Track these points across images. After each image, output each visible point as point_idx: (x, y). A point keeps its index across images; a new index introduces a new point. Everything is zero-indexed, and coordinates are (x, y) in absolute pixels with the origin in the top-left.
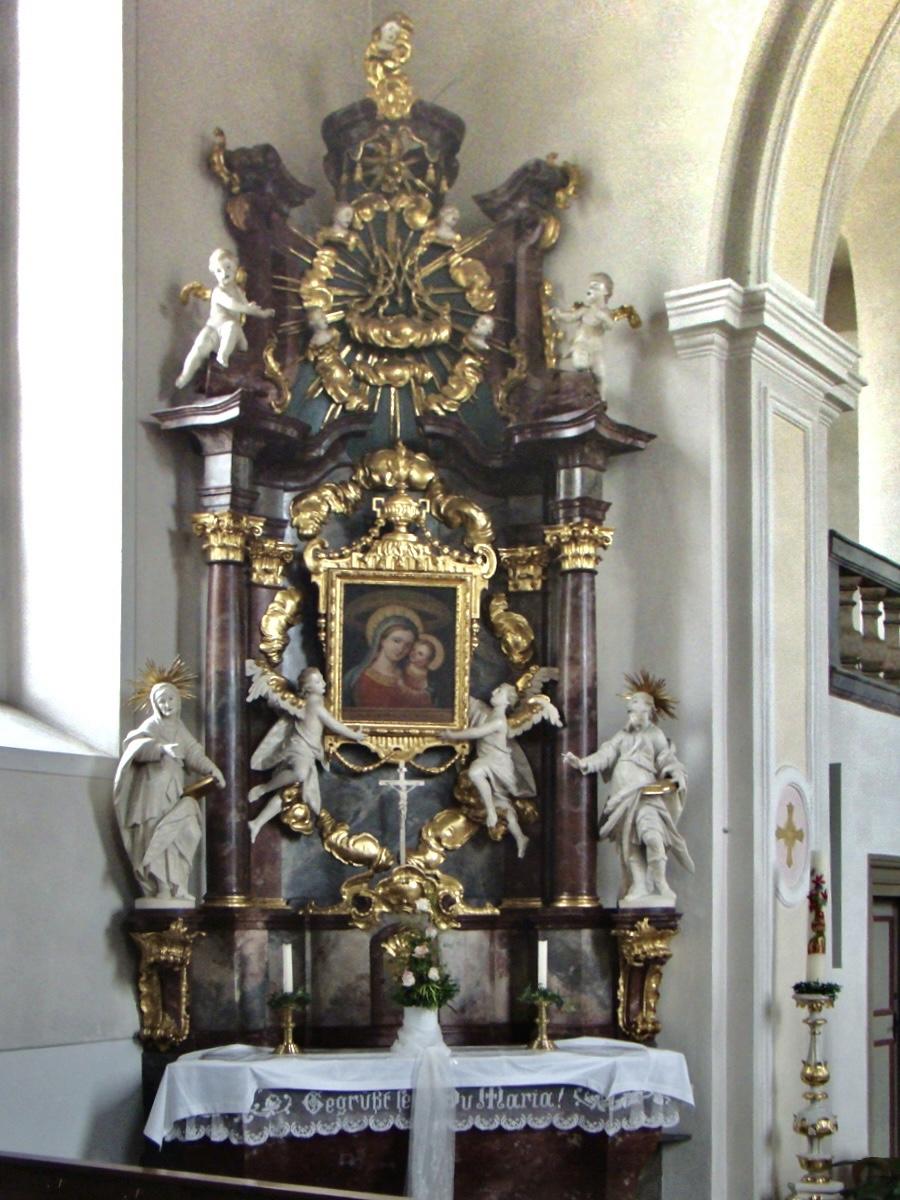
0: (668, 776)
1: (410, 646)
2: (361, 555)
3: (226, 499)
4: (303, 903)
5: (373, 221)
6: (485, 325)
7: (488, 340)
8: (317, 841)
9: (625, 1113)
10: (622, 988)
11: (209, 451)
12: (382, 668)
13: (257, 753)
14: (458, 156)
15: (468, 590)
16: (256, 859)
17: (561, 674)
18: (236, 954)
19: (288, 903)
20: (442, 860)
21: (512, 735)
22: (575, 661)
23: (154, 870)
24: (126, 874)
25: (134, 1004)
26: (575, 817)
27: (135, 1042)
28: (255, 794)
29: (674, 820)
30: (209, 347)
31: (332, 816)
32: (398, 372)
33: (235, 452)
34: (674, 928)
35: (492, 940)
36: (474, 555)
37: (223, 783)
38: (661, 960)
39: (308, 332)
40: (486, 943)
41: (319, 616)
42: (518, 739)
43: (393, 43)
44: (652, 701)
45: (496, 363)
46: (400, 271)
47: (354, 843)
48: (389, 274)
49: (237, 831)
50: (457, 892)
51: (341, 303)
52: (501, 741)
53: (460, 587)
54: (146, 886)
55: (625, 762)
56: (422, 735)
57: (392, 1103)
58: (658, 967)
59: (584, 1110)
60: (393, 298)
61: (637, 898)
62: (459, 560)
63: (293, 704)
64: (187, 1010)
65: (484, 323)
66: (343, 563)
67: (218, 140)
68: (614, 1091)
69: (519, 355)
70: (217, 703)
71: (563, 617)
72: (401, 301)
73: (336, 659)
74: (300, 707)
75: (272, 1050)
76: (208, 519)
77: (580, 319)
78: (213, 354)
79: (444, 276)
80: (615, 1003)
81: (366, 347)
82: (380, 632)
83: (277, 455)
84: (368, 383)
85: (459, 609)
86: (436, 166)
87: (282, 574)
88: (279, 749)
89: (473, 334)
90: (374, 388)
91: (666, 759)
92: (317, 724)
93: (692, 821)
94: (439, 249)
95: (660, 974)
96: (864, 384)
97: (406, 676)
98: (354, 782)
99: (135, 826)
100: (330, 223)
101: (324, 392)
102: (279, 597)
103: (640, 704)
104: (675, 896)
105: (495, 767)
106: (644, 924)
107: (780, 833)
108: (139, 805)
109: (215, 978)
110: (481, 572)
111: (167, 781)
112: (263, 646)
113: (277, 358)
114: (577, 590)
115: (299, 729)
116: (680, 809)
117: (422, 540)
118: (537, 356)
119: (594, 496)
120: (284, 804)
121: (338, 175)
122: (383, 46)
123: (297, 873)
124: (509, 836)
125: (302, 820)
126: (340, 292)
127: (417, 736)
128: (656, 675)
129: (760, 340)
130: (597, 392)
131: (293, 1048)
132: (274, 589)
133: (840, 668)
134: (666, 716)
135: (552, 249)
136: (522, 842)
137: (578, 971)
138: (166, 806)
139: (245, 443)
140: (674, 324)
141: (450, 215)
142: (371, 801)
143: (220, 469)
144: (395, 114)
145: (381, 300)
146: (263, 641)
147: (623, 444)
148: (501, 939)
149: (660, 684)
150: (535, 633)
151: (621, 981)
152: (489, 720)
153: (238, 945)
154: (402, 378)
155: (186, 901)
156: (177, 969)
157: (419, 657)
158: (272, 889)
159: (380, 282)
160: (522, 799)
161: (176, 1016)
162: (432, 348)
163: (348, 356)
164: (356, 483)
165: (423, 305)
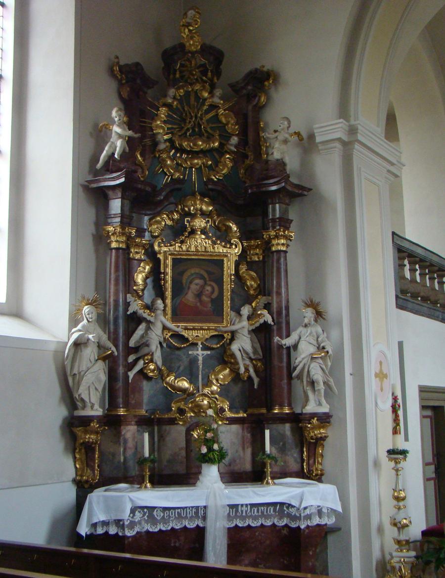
0: (324, 348)
1: (203, 287)
3: (118, 220)
6: (235, 140)
7: (236, 147)
8: (160, 381)
9: (309, 517)
12: (190, 297)
15: (229, 261)
19: (146, 412)
21: (251, 329)
22: (279, 293)
24: (70, 398)
25: (73, 464)
26: (280, 368)
27: (73, 483)
28: (131, 358)
30: (111, 151)
33: (123, 198)
34: (329, 422)
35: (243, 429)
36: (231, 244)
38: (323, 439)
39: (155, 144)
40: (240, 431)
41: (161, 273)
42: (253, 331)
44: (315, 312)
45: (240, 157)
48: (191, 118)
50: (226, 407)
51: (170, 131)
52: (246, 332)
54: (79, 404)
55: (304, 341)
56: (209, 329)
57: (197, 513)
58: (322, 442)
59: (289, 516)
61: (311, 408)
62: (224, 247)
63: (149, 315)
64: (98, 466)
66: (171, 248)
67: (116, 60)
68: (303, 506)
70: (113, 315)
73: (169, 294)
74: (152, 316)
75: (139, 486)
76: (111, 229)
77: (277, 137)
78: (113, 154)
81: (182, 150)
82: (189, 280)
83: (142, 198)
84: (182, 166)
88: (142, 337)
89: (229, 144)
90: (185, 168)
91: (322, 340)
93: (335, 371)
94: (214, 107)
97: (201, 301)
98: (177, 352)
99: (75, 374)
101: (163, 170)
102: (142, 264)
103: (309, 314)
105: (243, 344)
106: (315, 421)
107: (376, 375)
108: (77, 364)
111: (90, 353)
112: (135, 288)
113: (141, 156)
114: (278, 260)
116: (329, 364)
117: (208, 237)
118: (258, 154)
120: (145, 363)
124: (250, 378)
125: (153, 371)
127: (207, 330)
128: (316, 300)
129: (357, 146)
131: (149, 485)
132: (140, 261)
135: (264, 106)
136: (256, 381)
137: (284, 444)
138: (90, 365)
141: (218, 92)
142: (185, 361)
143: (116, 205)
144: (193, 49)
145: (188, 130)
146: (135, 286)
149: (318, 304)
151: (305, 449)
152: (239, 322)
153: (123, 433)
155: (98, 412)
156: (93, 446)
158: (139, 405)
159: (188, 121)
161: (93, 470)
162: (211, 150)
164: (177, 212)
165: (207, 132)
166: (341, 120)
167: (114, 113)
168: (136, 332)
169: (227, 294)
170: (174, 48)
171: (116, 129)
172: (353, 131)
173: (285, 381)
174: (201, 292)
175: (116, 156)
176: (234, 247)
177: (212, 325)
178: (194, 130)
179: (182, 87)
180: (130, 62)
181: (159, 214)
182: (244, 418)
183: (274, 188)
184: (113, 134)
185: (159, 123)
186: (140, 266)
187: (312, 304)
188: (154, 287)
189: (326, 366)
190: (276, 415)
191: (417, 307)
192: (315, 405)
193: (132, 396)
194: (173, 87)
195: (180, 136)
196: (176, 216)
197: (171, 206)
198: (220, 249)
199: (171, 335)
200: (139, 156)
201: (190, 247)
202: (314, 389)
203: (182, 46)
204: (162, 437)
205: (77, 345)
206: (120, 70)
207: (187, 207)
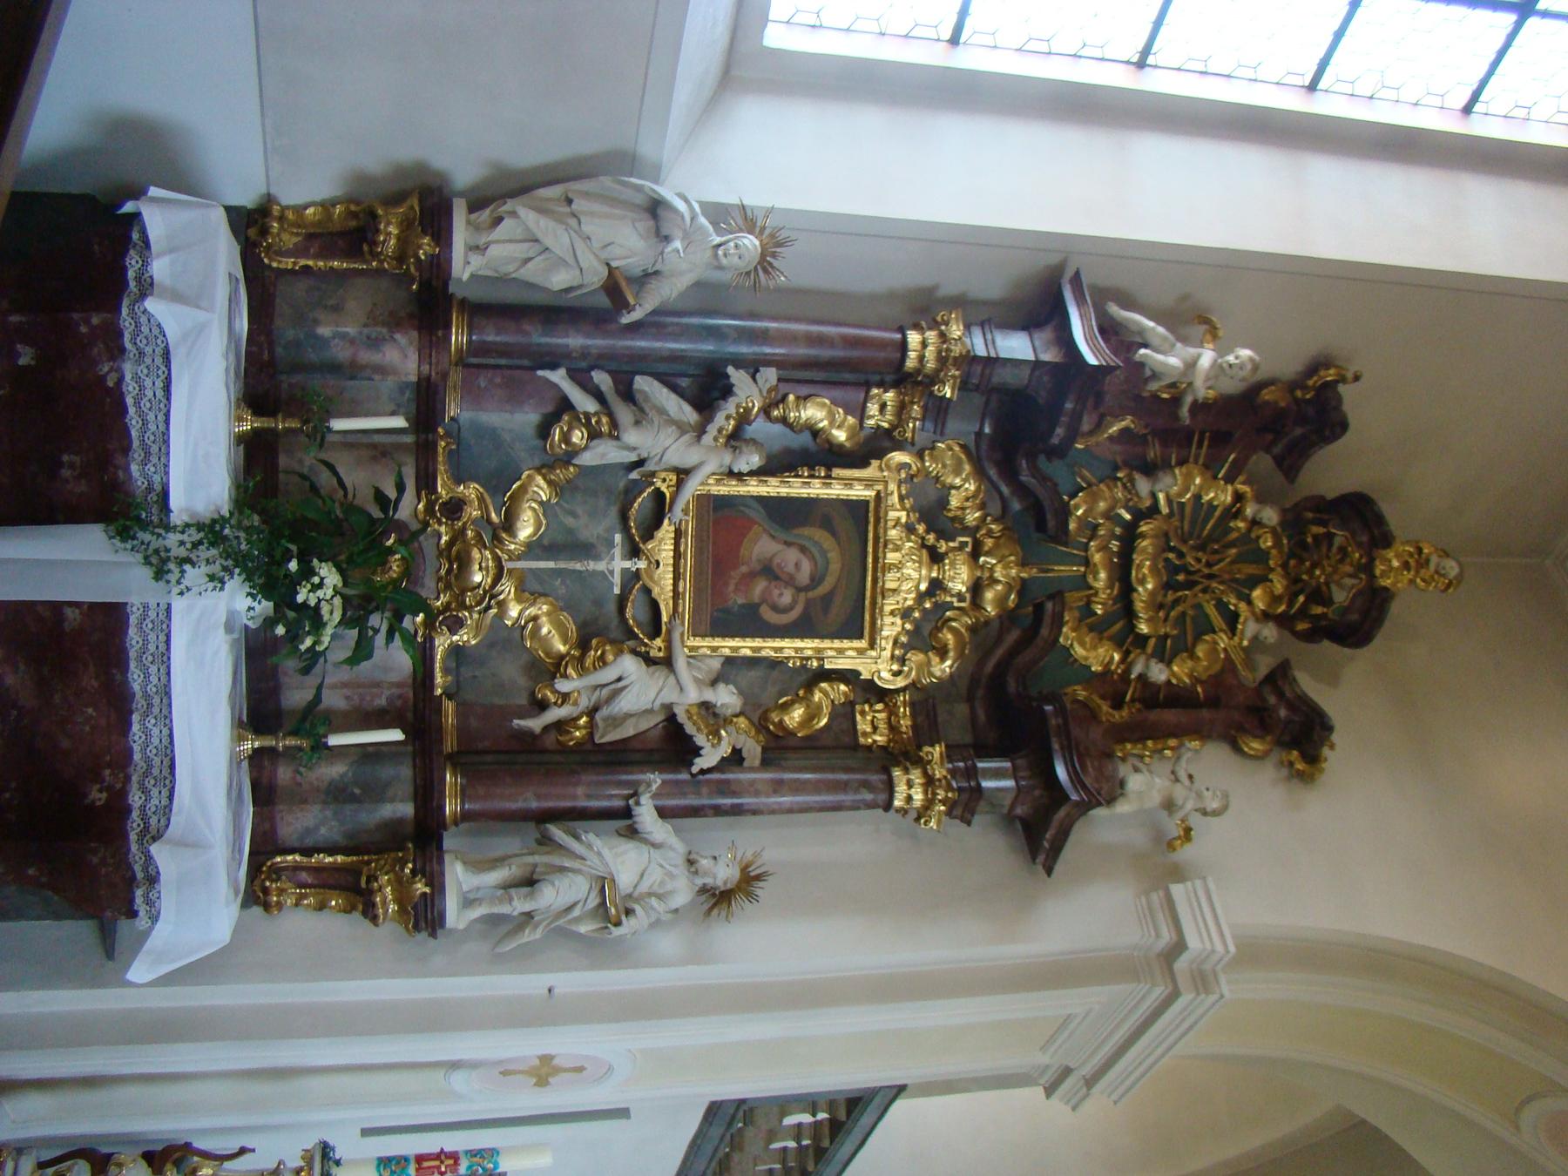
0: (629, 912)
1: (790, 582)
2: (903, 520)
3: (981, 350)
4: (455, 434)
5: (1260, 549)
6: (1158, 673)
7: (1141, 677)
8: (537, 463)
10: (329, 859)
11: (1036, 336)
12: (763, 546)
13: (656, 383)
14: (1326, 643)
15: (861, 652)
16: (514, 370)
17: (752, 769)
18: (384, 330)
19: (452, 419)
20: (509, 623)
21: (677, 710)
22: (778, 787)
23: (507, 223)
24: (498, 194)
27: (262, 196)
28: (602, 379)
29: (570, 922)
30: (1155, 341)
31: (568, 481)
32: (1103, 575)
33: (1037, 364)
34: (417, 927)
35: (399, 685)
37: (626, 319)
38: (370, 913)
39: (1150, 470)
40: (394, 677)
41: (829, 469)
42: (671, 718)
43: (1437, 572)
44: (729, 886)
45: (1113, 686)
46: (1210, 577)
47: (534, 509)
48: (1209, 565)
49: (558, 346)
50: (463, 637)
51: (1178, 509)
52: (670, 696)
53: (863, 644)
54: (485, 215)
55: (645, 860)
56: (676, 595)
58: (360, 907)
60: (1184, 569)
61: (458, 877)
62: (895, 642)
63: (720, 431)
64: (307, 267)
65: (1161, 671)
66: (895, 498)
67: (1350, 375)
69: (1125, 712)
70: (729, 326)
71: (833, 770)
72: (1181, 577)
73: (773, 488)
74: (716, 439)
76: (956, 331)
77: (1177, 780)
78: (1146, 346)
79: (1206, 628)
80: (307, 852)
81: (1130, 537)
82: (807, 544)
83: (1021, 429)
84: (1090, 540)
85: (837, 644)
86: (1324, 615)
87: (879, 427)
88: (662, 411)
89: (1147, 660)
90: (1086, 547)
91: (652, 908)
92: (694, 460)
94: (1232, 619)
95: (349, 909)
96: (1074, 1109)
97: (752, 575)
98: (614, 512)
99: (569, 201)
100: (1261, 499)
101: (1082, 489)
102: (851, 420)
103: (724, 874)
104: (461, 926)
105: (635, 689)
106: (421, 887)
107: (546, 1059)
108: (597, 207)
109: (351, 305)
110: (879, 666)
111: (627, 244)
112: (791, 397)
113: (1125, 431)
114: (866, 785)
115: (686, 437)
116: (583, 929)
117: (921, 597)
118: (1138, 732)
119: (982, 806)
120: (587, 416)
121: (1317, 510)
122: (1434, 560)
123: (492, 434)
124: (542, 706)
125: (566, 438)
126: (1188, 510)
128: (763, 890)
130: (1099, 804)
132: (862, 415)
133: (745, 1107)
134: (706, 907)
135: (1237, 749)
137: (354, 799)
138: (596, 245)
139: (1045, 378)
140: (1177, 890)
141: (1270, 632)
142: (589, 529)
143: (1016, 346)
144: (1379, 568)
145: (1181, 555)
146: (798, 398)
147: (1041, 833)
148: (400, 696)
149: (751, 896)
150: (806, 738)
151: (339, 858)
152: (697, 680)
153: (398, 336)
154: (1095, 578)
155: (465, 265)
156: (366, 248)
157: (776, 592)
158: (473, 395)
159: (1200, 554)
160: (591, 725)
161: (297, 252)
162: (1129, 613)
163: (1119, 515)
164: (983, 519)
165: (1176, 602)
166: (1232, 949)
167: (1245, 353)
168: (673, 396)
169: (769, 647)
170: (1380, 520)
171: (1207, 358)
172: (1203, 981)
173: (534, 805)
174: (777, 578)
175: (1142, 351)
176: (895, 667)
177: (687, 604)
178: (1176, 570)
179: (1277, 543)
180: (1347, 407)
181: (980, 472)
182: (432, 687)
183: (1061, 772)
184: (1192, 351)
185: (1198, 481)
186: (846, 413)
187: (748, 882)
188: (788, 452)
189: (577, 920)
190: (422, 796)
191: (708, 1149)
192: (465, 888)
193: (498, 380)
194: (1283, 523)
195: (1166, 535)
196: (972, 517)
197: (999, 504)
198: (891, 628)
199: (663, 494)
200: (1123, 424)
201: (897, 549)
202: (510, 886)
203: (1386, 540)
204: (384, 454)
205: (655, 208)
206: (1326, 385)
207: (997, 546)
